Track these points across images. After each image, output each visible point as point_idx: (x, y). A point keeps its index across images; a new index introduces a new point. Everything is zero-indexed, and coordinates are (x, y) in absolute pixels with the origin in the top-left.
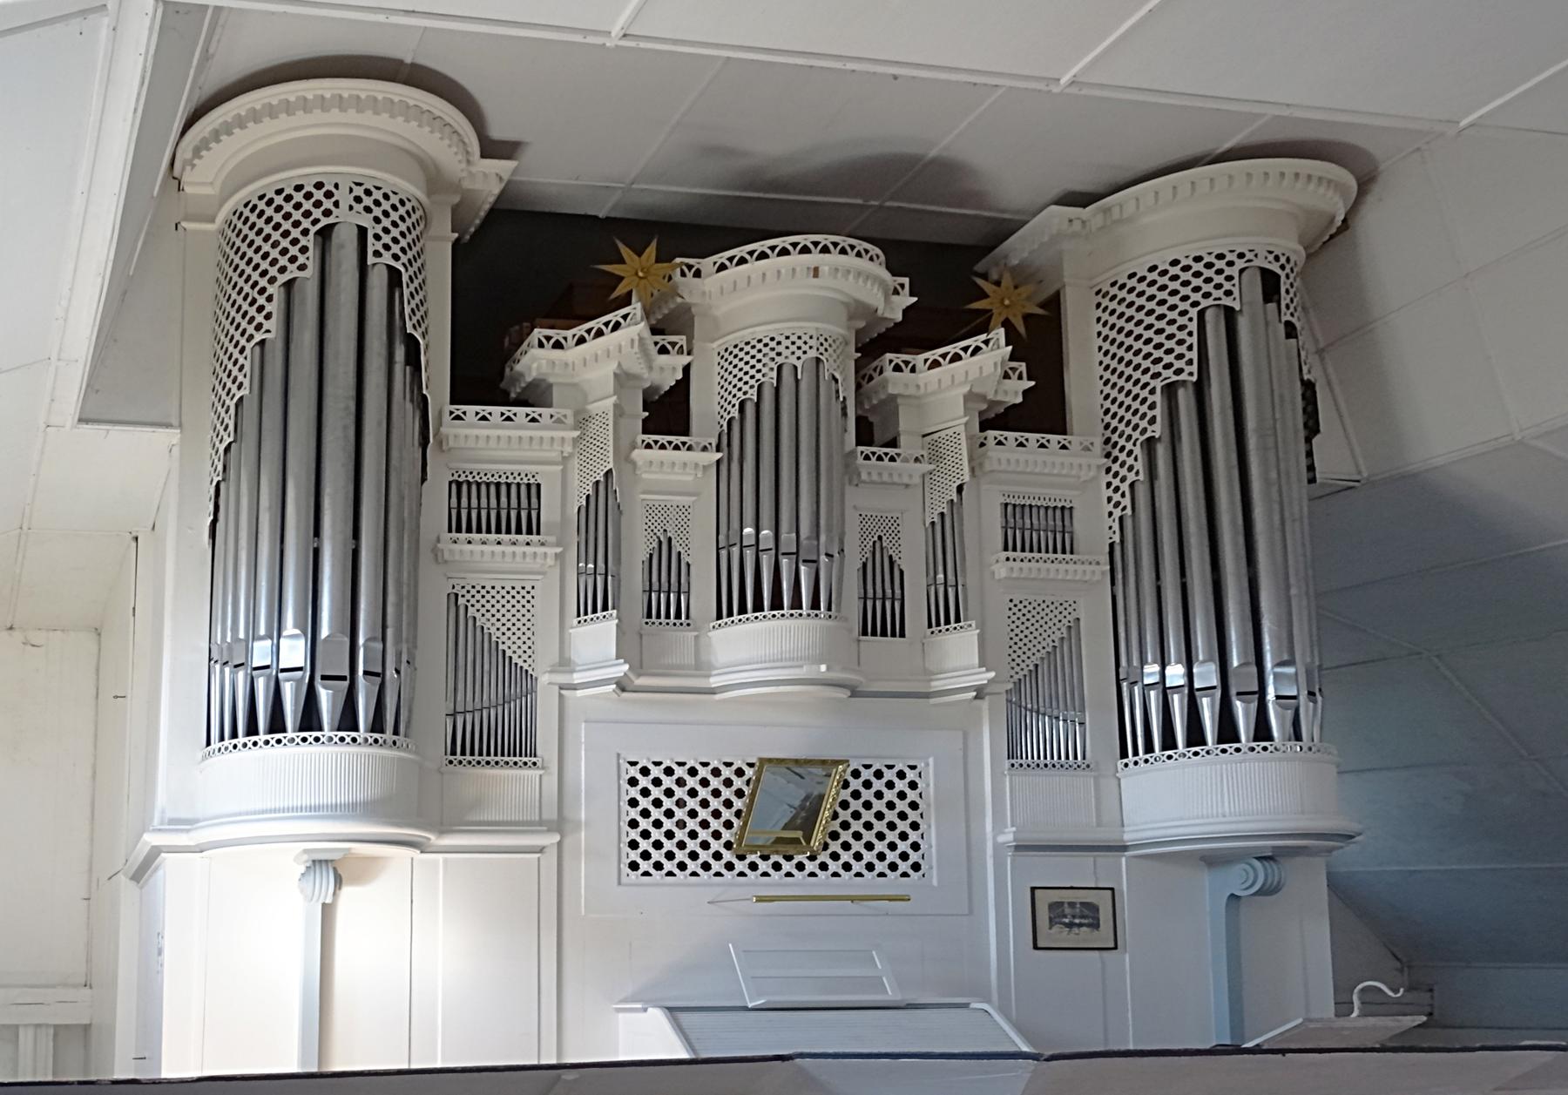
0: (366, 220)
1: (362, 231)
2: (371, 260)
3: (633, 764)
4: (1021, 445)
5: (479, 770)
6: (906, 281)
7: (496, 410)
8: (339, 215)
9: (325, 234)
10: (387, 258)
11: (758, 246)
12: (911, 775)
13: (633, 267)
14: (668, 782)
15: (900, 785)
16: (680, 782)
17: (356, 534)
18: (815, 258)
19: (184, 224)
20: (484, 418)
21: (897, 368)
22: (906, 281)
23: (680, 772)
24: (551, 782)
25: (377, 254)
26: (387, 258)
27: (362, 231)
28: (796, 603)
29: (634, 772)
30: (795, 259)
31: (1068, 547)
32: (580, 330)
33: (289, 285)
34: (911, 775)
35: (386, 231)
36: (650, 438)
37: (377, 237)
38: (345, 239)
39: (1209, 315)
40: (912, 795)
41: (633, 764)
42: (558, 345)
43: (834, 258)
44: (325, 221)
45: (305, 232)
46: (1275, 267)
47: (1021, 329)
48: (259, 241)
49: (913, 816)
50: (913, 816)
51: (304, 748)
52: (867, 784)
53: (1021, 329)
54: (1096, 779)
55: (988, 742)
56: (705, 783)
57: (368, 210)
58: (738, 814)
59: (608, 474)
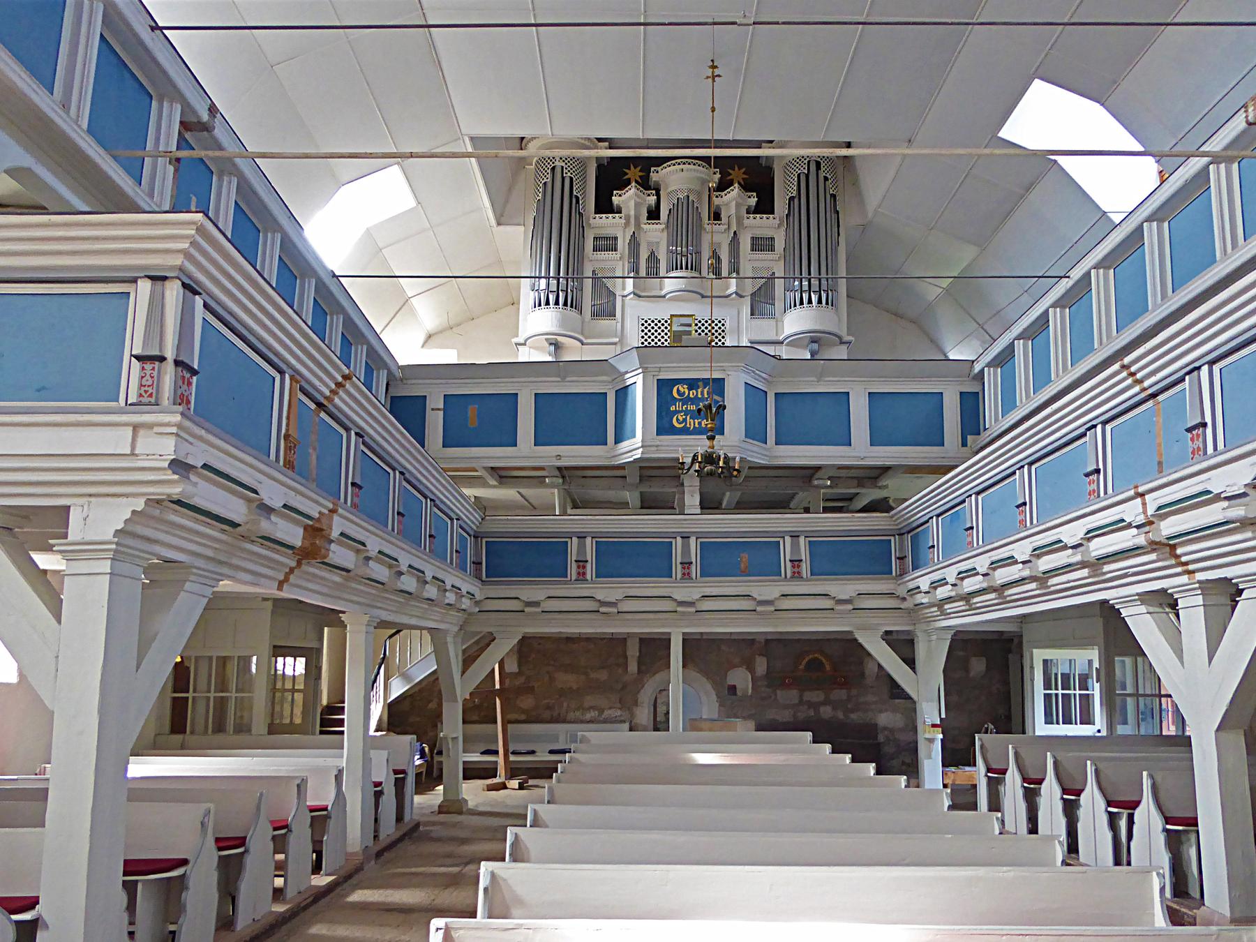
0: (563, 164)
1: (562, 167)
2: (564, 175)
3: (643, 319)
4: (754, 218)
5: (600, 321)
6: (718, 170)
7: (610, 215)
8: (557, 163)
9: (553, 169)
10: (569, 174)
11: (669, 163)
12: (723, 322)
13: (634, 173)
14: (653, 325)
15: (720, 325)
16: (656, 325)
17: (560, 252)
18: (681, 166)
19: (526, 167)
20: (601, 218)
21: (717, 197)
22: (718, 170)
23: (656, 322)
24: (619, 325)
25: (566, 173)
26: (569, 174)
27: (562, 167)
28: (681, 268)
29: (643, 322)
30: (677, 167)
31: (773, 250)
32: (726, 192)
33: (545, 183)
34: (723, 322)
35: (569, 166)
36: (649, 221)
37: (566, 168)
38: (558, 171)
39: (801, 175)
40: (723, 328)
41: (643, 319)
42: (620, 196)
43: (687, 166)
44: (553, 165)
45: (548, 169)
46: (819, 160)
47: (639, 180)
48: (544, 172)
49: (723, 334)
50: (723, 334)
51: (546, 309)
52: (703, 325)
53: (639, 180)
54: (777, 321)
55: (746, 310)
56: (656, 325)
57: (564, 161)
58: (669, 331)
59: (634, 233)
